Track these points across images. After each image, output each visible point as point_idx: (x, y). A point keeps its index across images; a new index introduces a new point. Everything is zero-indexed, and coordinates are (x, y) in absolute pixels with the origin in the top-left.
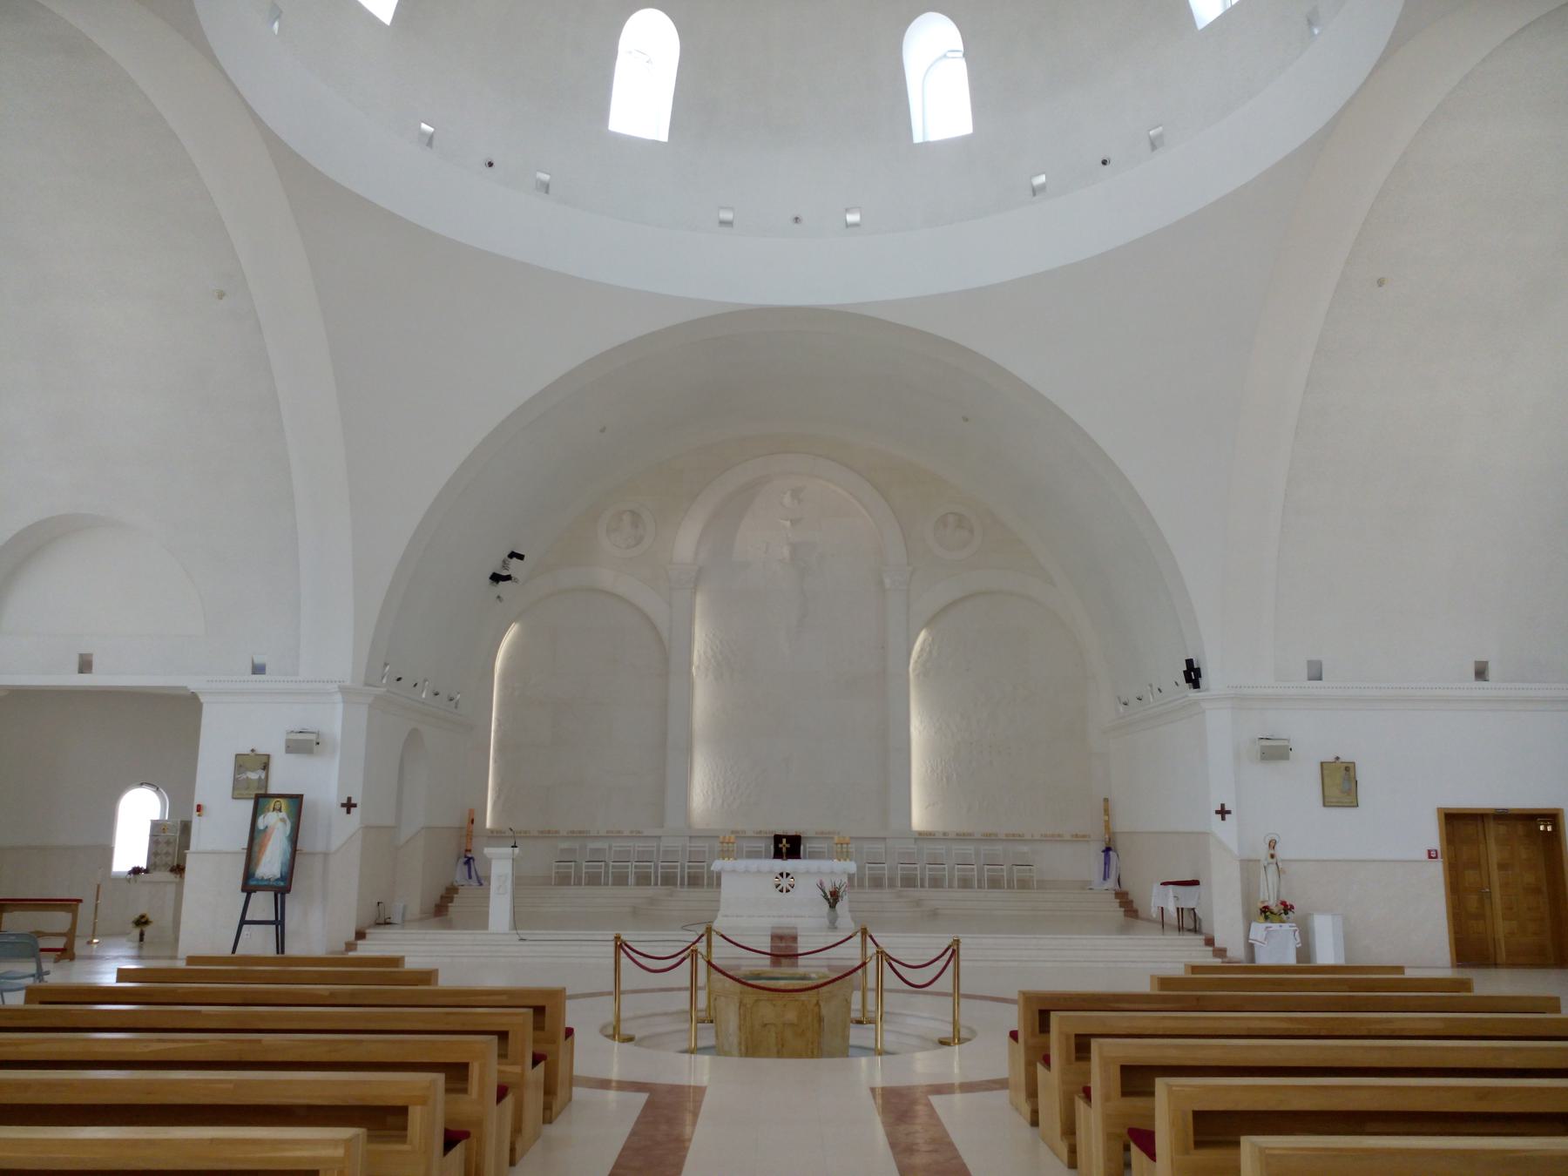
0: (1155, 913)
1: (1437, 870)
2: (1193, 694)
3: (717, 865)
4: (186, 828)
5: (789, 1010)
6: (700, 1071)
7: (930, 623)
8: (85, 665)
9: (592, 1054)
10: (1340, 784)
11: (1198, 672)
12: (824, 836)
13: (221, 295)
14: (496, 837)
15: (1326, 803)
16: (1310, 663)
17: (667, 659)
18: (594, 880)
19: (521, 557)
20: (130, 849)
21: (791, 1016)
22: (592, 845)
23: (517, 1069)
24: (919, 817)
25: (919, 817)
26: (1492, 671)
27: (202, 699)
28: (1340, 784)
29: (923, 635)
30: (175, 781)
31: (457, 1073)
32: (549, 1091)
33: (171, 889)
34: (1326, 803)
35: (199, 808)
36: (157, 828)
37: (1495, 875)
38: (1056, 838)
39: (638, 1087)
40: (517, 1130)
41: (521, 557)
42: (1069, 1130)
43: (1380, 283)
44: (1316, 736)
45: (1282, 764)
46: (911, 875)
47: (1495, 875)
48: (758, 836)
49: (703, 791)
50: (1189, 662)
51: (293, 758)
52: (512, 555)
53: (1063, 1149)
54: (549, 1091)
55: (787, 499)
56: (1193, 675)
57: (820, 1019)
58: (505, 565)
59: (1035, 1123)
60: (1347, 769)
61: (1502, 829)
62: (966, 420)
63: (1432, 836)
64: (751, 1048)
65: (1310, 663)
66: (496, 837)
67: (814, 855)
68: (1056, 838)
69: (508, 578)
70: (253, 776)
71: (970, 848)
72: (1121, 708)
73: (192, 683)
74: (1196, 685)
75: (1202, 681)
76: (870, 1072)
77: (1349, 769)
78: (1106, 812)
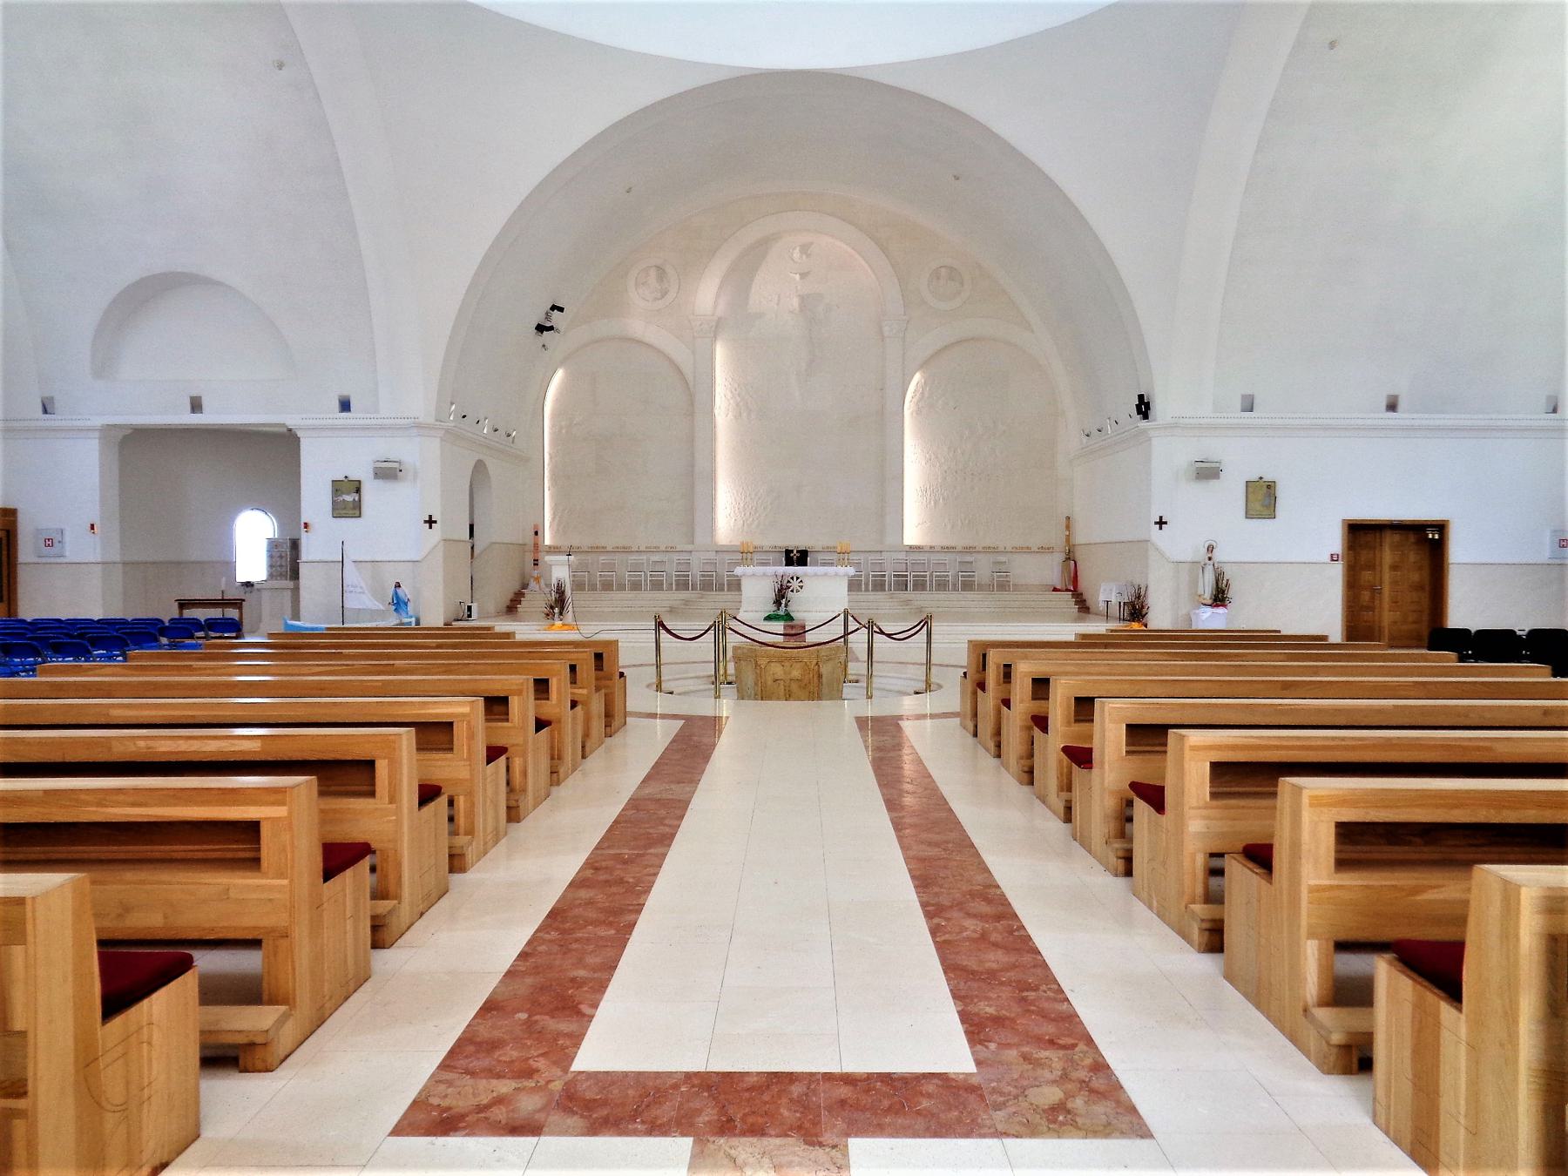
0: (1102, 606)
1: (1338, 570)
2: (1144, 424)
3: (739, 571)
4: (295, 545)
5: (794, 668)
6: (726, 707)
7: (923, 366)
8: (196, 405)
9: (638, 696)
10: (1262, 498)
11: (1148, 405)
12: (830, 550)
13: (280, 66)
14: (554, 550)
15: (1248, 516)
16: (1244, 397)
17: (693, 398)
18: (636, 586)
19: (561, 310)
20: (251, 564)
21: (796, 673)
22: (656, 558)
23: (585, 691)
24: (914, 532)
25: (914, 532)
26: (1402, 405)
27: (299, 434)
28: (1262, 498)
29: (917, 377)
30: (285, 502)
31: (542, 686)
32: (609, 715)
33: (288, 595)
34: (1248, 516)
35: (306, 525)
36: (273, 545)
37: (1387, 576)
38: (1026, 550)
39: (675, 717)
40: (586, 735)
41: (561, 310)
42: (998, 733)
43: (1332, 45)
44: (1243, 461)
45: (1213, 483)
46: (909, 578)
47: (1387, 576)
48: (774, 550)
49: (727, 517)
50: (1141, 397)
51: (380, 483)
52: (554, 308)
53: (991, 745)
54: (609, 715)
55: (796, 254)
56: (1144, 408)
57: (820, 676)
58: (548, 317)
59: (975, 735)
60: (1269, 487)
61: (1397, 537)
62: (957, 178)
63: (1335, 541)
64: (764, 694)
65: (1244, 397)
66: (554, 550)
67: (815, 564)
68: (1026, 550)
69: (551, 328)
70: (349, 498)
71: (947, 558)
72: (1085, 439)
73: (291, 421)
74: (1146, 416)
75: (1151, 414)
76: (853, 705)
77: (1270, 487)
78: (1068, 527)
